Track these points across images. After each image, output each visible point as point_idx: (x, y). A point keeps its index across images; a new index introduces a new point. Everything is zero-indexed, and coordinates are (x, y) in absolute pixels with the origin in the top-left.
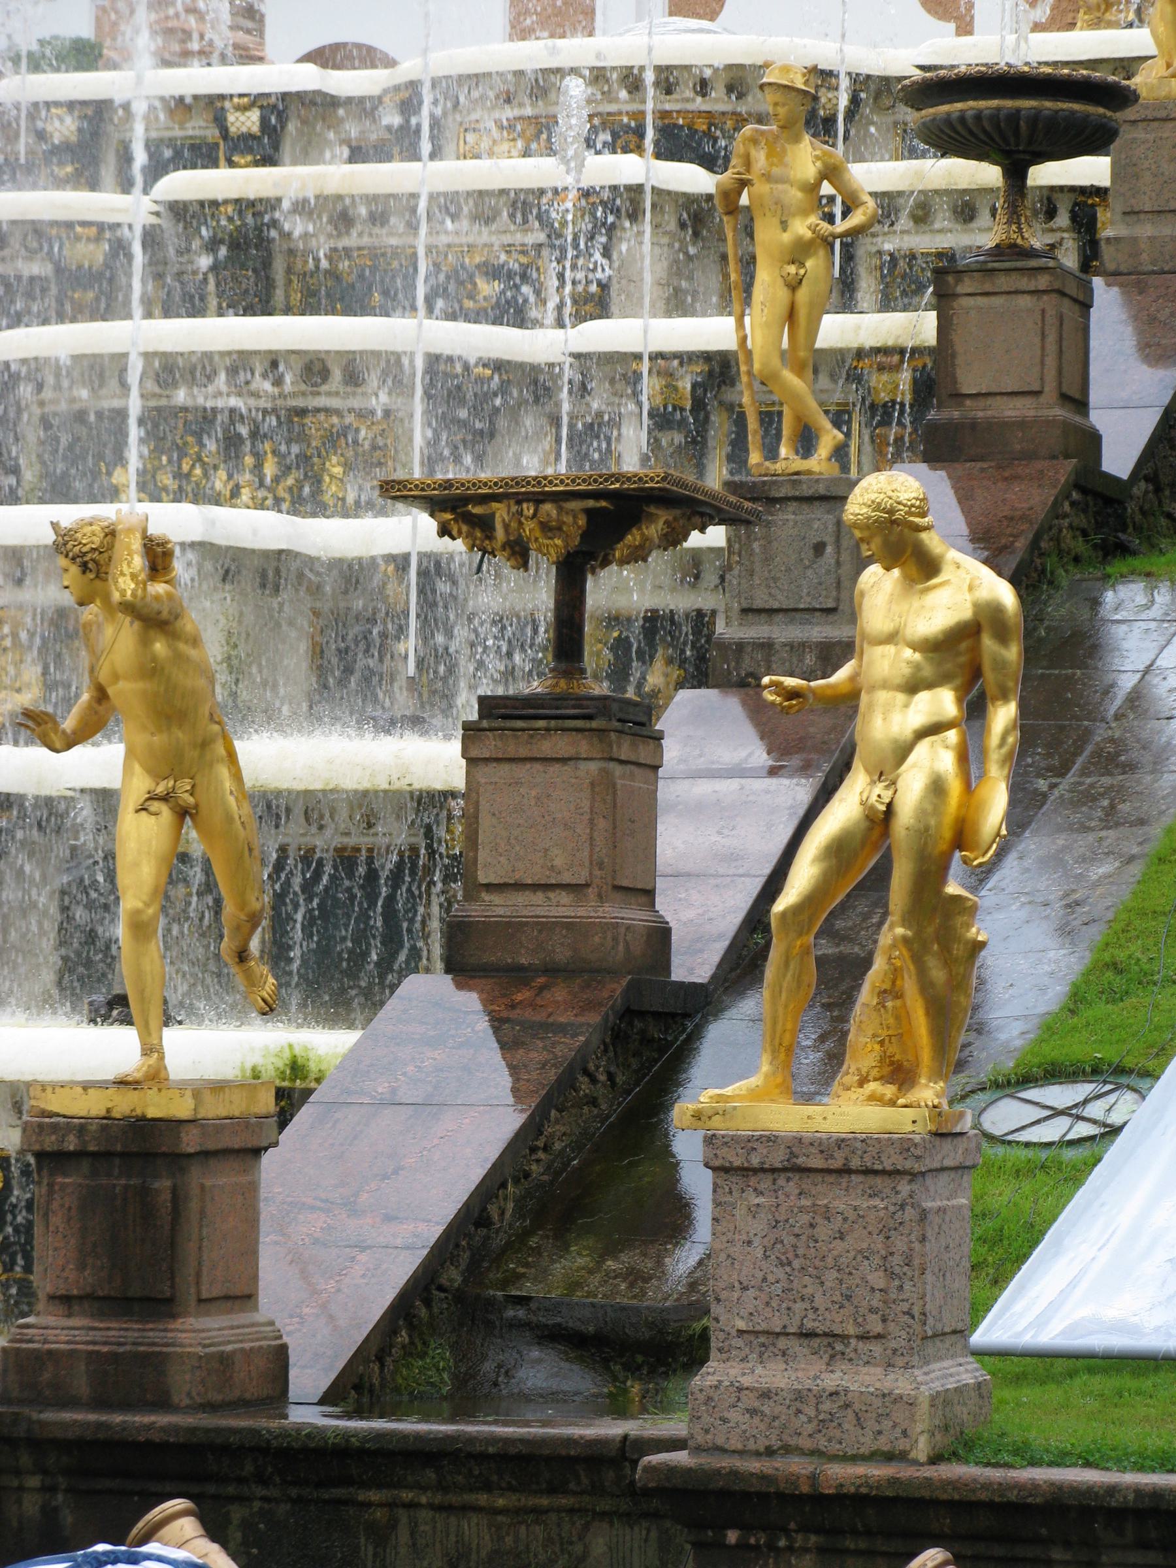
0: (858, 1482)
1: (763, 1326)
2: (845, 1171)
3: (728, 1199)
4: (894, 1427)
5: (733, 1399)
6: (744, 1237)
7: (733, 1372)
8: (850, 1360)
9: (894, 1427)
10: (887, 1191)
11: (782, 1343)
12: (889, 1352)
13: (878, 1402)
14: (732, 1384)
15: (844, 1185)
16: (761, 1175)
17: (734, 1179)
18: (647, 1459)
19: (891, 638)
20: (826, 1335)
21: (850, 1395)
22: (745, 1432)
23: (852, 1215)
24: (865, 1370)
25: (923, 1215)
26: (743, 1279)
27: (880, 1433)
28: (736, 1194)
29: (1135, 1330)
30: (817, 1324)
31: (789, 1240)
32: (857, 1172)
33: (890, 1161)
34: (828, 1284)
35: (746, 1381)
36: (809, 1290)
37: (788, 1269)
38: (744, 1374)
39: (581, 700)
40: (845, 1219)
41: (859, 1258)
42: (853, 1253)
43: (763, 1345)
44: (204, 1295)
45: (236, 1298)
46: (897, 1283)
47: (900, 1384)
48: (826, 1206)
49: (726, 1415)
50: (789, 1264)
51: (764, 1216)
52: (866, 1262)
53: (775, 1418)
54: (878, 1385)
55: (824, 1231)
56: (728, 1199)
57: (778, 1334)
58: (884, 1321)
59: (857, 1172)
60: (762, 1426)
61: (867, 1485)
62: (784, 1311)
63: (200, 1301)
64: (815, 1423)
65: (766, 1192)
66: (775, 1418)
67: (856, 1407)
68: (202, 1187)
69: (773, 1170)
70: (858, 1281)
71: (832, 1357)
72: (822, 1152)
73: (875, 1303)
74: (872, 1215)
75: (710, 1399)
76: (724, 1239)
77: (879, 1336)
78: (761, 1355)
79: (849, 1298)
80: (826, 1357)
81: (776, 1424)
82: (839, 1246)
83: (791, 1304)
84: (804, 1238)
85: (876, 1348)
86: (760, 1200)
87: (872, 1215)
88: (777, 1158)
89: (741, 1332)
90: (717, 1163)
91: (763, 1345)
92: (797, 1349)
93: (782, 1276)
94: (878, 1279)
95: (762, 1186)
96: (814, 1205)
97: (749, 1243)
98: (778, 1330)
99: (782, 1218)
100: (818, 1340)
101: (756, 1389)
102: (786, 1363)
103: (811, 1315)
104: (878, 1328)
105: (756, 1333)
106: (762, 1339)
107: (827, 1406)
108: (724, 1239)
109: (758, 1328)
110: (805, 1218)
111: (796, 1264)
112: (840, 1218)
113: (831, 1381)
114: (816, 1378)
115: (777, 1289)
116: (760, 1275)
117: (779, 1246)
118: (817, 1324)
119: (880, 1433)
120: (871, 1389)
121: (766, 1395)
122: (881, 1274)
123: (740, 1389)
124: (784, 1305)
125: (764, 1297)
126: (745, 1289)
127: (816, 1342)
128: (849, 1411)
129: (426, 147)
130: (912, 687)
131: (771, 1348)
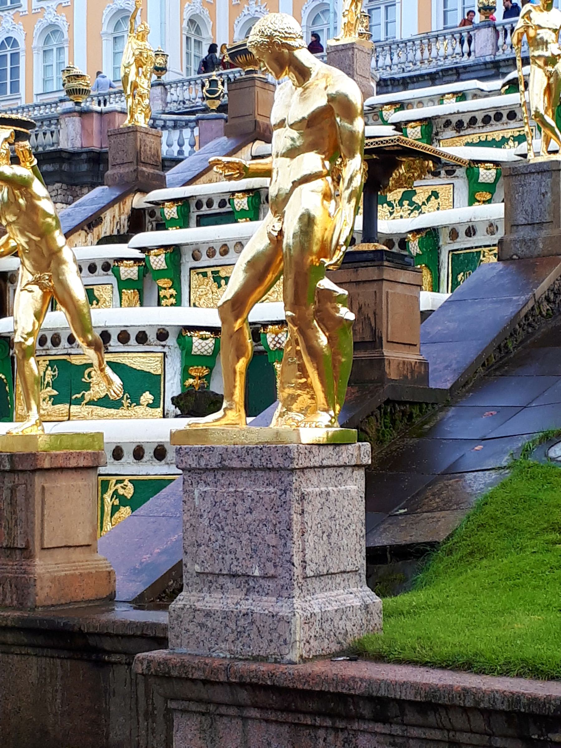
0: (252, 675)
1: (210, 570)
2: (251, 469)
3: (191, 488)
4: (279, 637)
5: (191, 617)
6: (199, 513)
7: (192, 599)
8: (258, 592)
9: (279, 637)
10: (277, 481)
11: (221, 580)
12: (279, 587)
13: (270, 621)
14: (191, 607)
15: (253, 478)
16: (208, 472)
17: (194, 476)
18: (139, 655)
19: (282, 124)
20: (243, 575)
21: (254, 615)
22: (197, 638)
23: (256, 498)
24: (265, 598)
25: (303, 497)
26: (198, 540)
27: (271, 641)
28: (194, 485)
29: (136, 593)
30: (238, 568)
31: (222, 514)
32: (259, 469)
33: (276, 462)
34: (244, 542)
35: (199, 605)
36: (234, 546)
37: (222, 532)
38: (198, 601)
39: (393, 253)
40: (253, 500)
41: (261, 525)
42: (257, 522)
43: (211, 582)
44: (45, 546)
45: (70, 547)
46: (283, 541)
47: (284, 609)
48: (242, 492)
49: (187, 627)
50: (223, 529)
51: (209, 499)
52: (265, 528)
53: (214, 630)
54: (271, 609)
55: (240, 509)
56: (191, 488)
57: (218, 575)
58: (275, 566)
59: (259, 469)
60: (207, 635)
61: (256, 676)
62: (221, 560)
63: (43, 549)
64: (236, 633)
65: (211, 484)
66: (214, 630)
67: (258, 623)
68: (43, 488)
69: (214, 470)
70: (260, 540)
71: (248, 590)
72: (239, 457)
73: (270, 555)
74: (267, 498)
75: (179, 616)
76: (189, 513)
77: (273, 577)
78: (210, 587)
79: (255, 551)
80: (245, 590)
81: (214, 633)
82: (250, 518)
83: (224, 556)
84: (231, 512)
85: (271, 584)
86: (208, 488)
87: (267, 498)
88: (214, 462)
89: (198, 574)
90: (183, 465)
91: (211, 582)
92: (229, 584)
93: (219, 538)
94: (272, 539)
95: (209, 480)
96: (236, 491)
97: (201, 516)
98: (217, 572)
99: (218, 500)
100: (241, 578)
101: (204, 611)
102: (223, 593)
103: (235, 563)
104: (272, 572)
105: (207, 574)
106: (210, 578)
107: (242, 622)
108: (189, 513)
109: (206, 571)
110: (231, 500)
111: (226, 529)
112: (250, 499)
113: (245, 606)
114: (238, 603)
115: (217, 545)
116: (207, 537)
117: (217, 518)
118: (238, 568)
119: (271, 641)
120: (266, 612)
121: (208, 614)
122: (274, 536)
123: (195, 610)
124: (220, 556)
125: (209, 551)
126: (199, 545)
127: (238, 580)
128: (254, 626)
129: (522, 87)
130: (292, 153)
131: (215, 584)
